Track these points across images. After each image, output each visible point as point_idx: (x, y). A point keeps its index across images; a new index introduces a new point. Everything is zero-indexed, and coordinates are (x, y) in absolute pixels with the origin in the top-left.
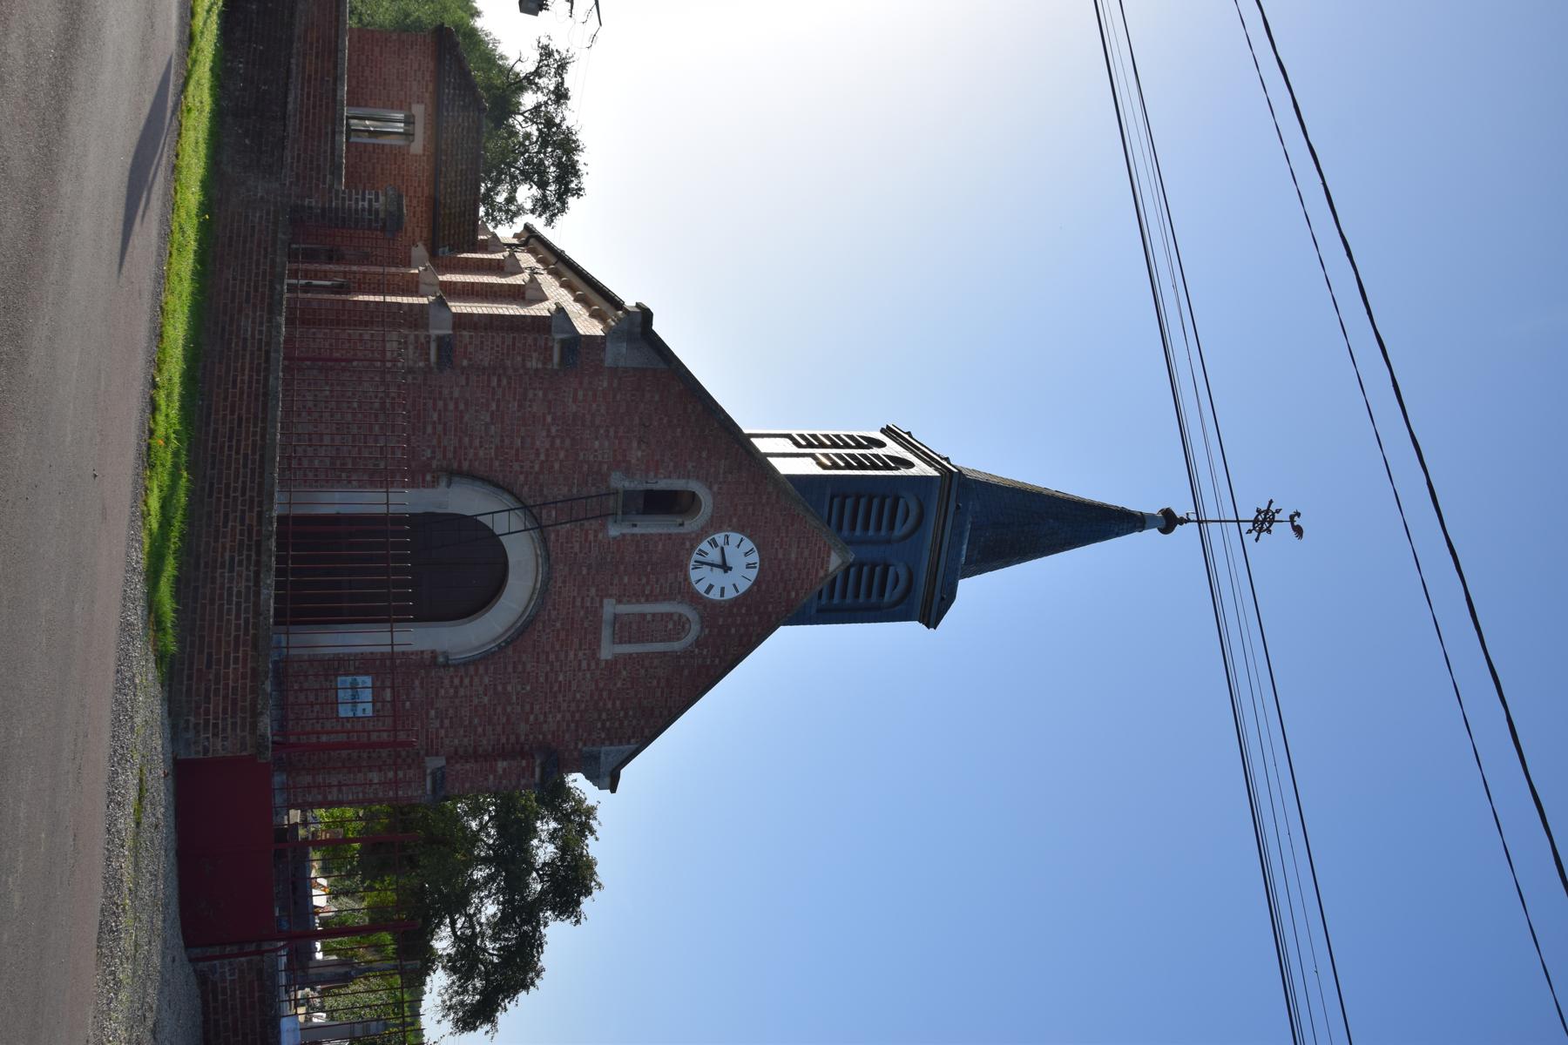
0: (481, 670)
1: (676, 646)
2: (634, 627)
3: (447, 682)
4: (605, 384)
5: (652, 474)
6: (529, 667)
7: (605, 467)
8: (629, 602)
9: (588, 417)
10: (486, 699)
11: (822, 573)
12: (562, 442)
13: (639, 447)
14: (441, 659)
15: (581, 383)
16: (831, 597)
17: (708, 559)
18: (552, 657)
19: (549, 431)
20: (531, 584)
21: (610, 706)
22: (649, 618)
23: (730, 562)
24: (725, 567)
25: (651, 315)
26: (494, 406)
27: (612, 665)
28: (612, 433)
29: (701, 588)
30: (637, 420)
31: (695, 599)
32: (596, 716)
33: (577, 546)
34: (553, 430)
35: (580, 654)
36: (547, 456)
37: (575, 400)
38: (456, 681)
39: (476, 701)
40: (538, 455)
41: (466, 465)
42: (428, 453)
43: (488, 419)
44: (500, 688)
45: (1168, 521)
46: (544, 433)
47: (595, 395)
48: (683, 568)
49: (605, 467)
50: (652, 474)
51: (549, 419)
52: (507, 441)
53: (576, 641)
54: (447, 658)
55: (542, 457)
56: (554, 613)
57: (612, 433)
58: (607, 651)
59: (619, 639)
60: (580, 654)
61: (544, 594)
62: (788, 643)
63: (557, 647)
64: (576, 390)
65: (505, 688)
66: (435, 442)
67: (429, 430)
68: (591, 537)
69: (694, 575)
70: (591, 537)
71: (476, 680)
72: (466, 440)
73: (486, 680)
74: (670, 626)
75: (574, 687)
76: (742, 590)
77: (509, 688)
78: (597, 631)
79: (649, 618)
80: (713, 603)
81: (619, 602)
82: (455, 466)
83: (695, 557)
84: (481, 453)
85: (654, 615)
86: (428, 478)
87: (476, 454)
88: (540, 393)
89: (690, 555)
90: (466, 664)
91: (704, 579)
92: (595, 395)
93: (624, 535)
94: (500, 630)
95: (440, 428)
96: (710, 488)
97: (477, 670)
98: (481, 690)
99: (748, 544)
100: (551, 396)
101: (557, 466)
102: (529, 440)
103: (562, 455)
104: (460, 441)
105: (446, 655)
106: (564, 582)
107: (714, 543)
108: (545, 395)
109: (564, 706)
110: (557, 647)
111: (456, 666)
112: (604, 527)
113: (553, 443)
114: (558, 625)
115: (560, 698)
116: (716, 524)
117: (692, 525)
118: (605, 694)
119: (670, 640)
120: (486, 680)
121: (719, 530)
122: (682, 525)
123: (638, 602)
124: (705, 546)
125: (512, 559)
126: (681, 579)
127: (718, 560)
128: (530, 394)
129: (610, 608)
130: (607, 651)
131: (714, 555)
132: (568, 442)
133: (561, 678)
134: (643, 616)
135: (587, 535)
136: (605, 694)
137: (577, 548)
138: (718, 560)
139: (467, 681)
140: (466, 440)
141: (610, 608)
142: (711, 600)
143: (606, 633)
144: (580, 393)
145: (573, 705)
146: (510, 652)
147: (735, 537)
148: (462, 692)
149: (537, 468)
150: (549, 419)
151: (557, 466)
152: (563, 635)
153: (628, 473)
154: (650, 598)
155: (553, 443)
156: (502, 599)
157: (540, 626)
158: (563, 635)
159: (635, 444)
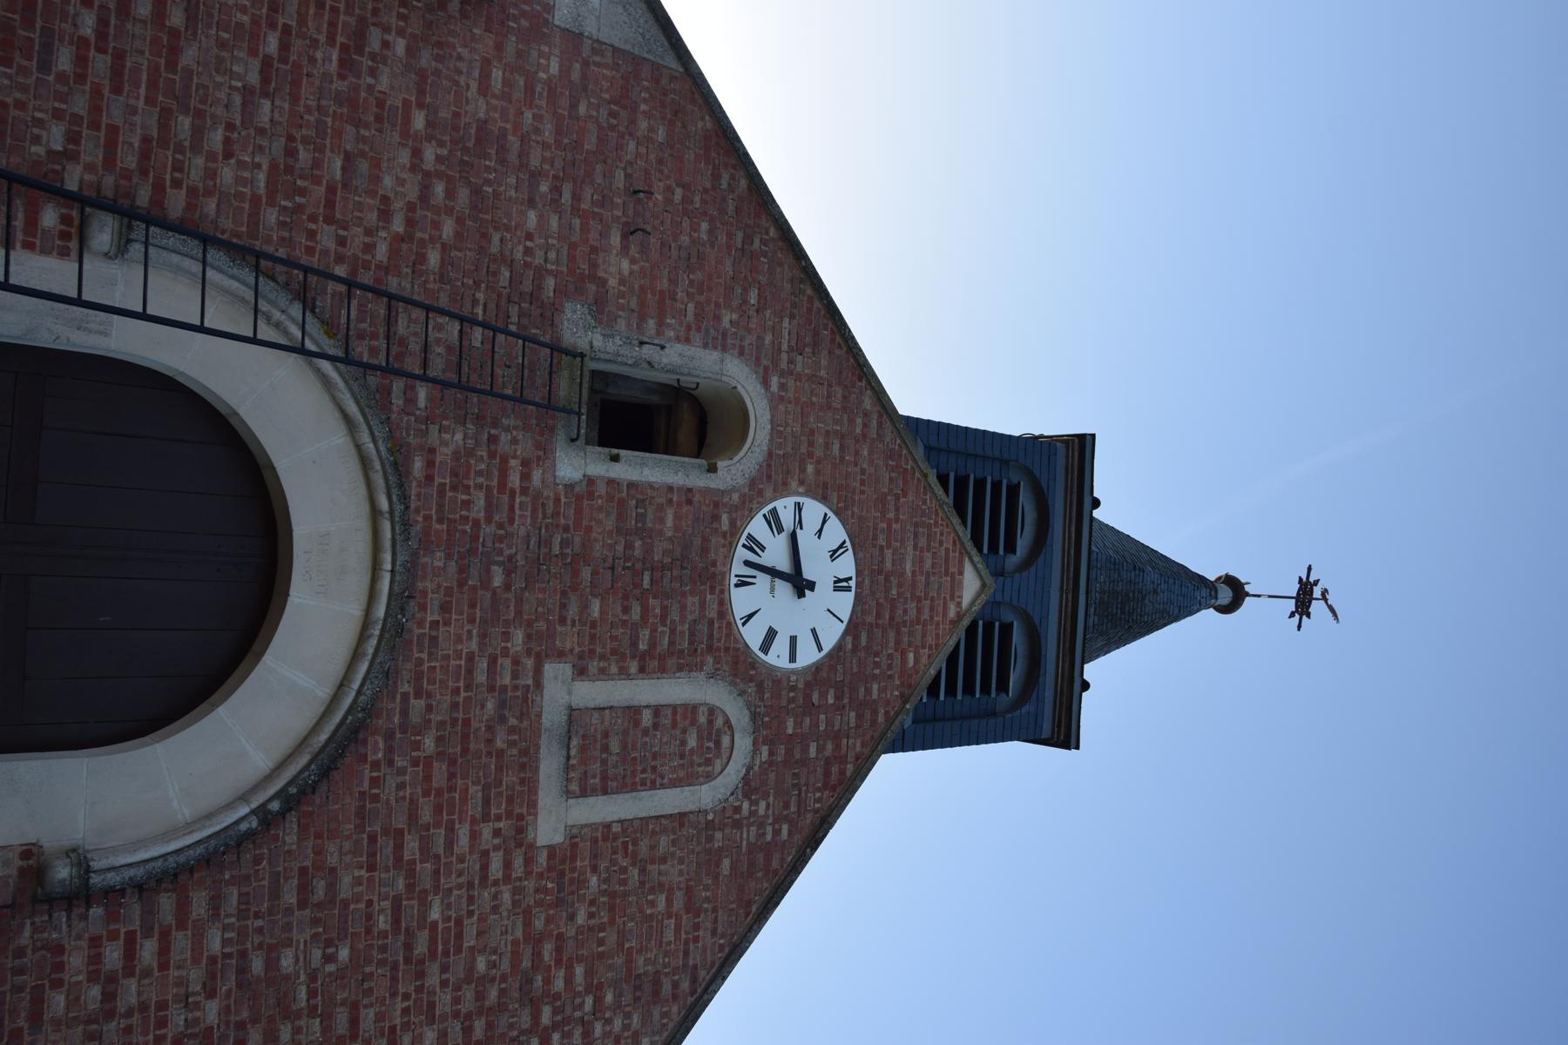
0: (199, 904)
1: (705, 796)
2: (615, 747)
3: (76, 961)
4: (554, 68)
5: (651, 324)
6: (345, 888)
7: (550, 283)
8: (603, 674)
9: (514, 142)
10: (211, 1011)
11: (952, 614)
12: (450, 194)
13: (625, 249)
14: (62, 872)
15: (499, 47)
16: (951, 691)
17: (766, 559)
18: (411, 846)
19: (417, 153)
20: (356, 610)
21: (559, 984)
22: (647, 718)
23: (808, 574)
24: (801, 586)
25: (1227, 576)
26: (272, 44)
27: (563, 856)
28: (566, 197)
29: (752, 636)
30: (619, 180)
31: (740, 666)
32: (525, 1020)
33: (480, 501)
34: (429, 154)
35: (486, 831)
36: (410, 223)
37: (484, 90)
38: (113, 955)
39: (178, 1019)
40: (385, 215)
41: (176, 204)
42: (56, 137)
43: (254, 78)
44: (257, 965)
46: (404, 157)
47: (530, 90)
48: (713, 581)
49: (550, 283)
50: (651, 324)
51: (419, 121)
52: (304, 156)
53: (475, 791)
54: (83, 865)
55: (398, 226)
56: (418, 705)
57: (566, 197)
59: (581, 786)
60: (486, 831)
61: (391, 637)
62: (901, 784)
63: (426, 815)
64: (486, 64)
65: (272, 964)
66: (80, 105)
67: (64, 60)
68: (515, 480)
69: (741, 602)
70: (515, 480)
71: (181, 942)
72: (184, 123)
73: (215, 943)
74: (692, 742)
75: (469, 941)
76: (829, 643)
77: (287, 962)
78: (528, 763)
79: (647, 718)
81: (581, 672)
82: (143, 197)
83: (741, 553)
84: (227, 174)
85: (657, 710)
86: (49, 217)
87: (211, 174)
88: (400, 46)
89: (731, 548)
90: (150, 884)
92: (530, 90)
93: (591, 481)
94: (261, 762)
95: (100, 64)
96: (765, 383)
97: (183, 907)
98: (196, 976)
100: (425, 59)
101: (434, 258)
102: (363, 166)
103: (448, 229)
104: (164, 125)
105: (79, 858)
106: (445, 608)
107: (774, 521)
108: (411, 51)
109: (444, 1000)
110: (426, 815)
111: (112, 895)
112: (544, 452)
113: (426, 190)
114: (429, 743)
115: (433, 980)
116: (775, 477)
117: (734, 471)
118: (548, 949)
119: (690, 779)
120: (215, 943)
121: (782, 490)
122: (615, 459)
123: (624, 673)
124: (757, 527)
126: (712, 613)
127: (784, 565)
128: (374, 40)
129: (562, 691)
131: (776, 553)
132: (463, 195)
133: (435, 914)
134: (633, 711)
135: (504, 473)
136: (548, 949)
137: (478, 509)
138: (784, 565)
139: (148, 951)
140: (184, 123)
141: (562, 691)
142: (772, 669)
143: (549, 766)
144: (497, 74)
145: (469, 994)
146: (289, 835)
147: (814, 510)
148: (130, 991)
149: (382, 253)
150: (419, 121)
151: (434, 258)
152: (440, 771)
153: (600, 310)
154: (652, 663)
155: (426, 190)
156: (268, 659)
157: (377, 747)
158: (440, 771)
159: (616, 239)
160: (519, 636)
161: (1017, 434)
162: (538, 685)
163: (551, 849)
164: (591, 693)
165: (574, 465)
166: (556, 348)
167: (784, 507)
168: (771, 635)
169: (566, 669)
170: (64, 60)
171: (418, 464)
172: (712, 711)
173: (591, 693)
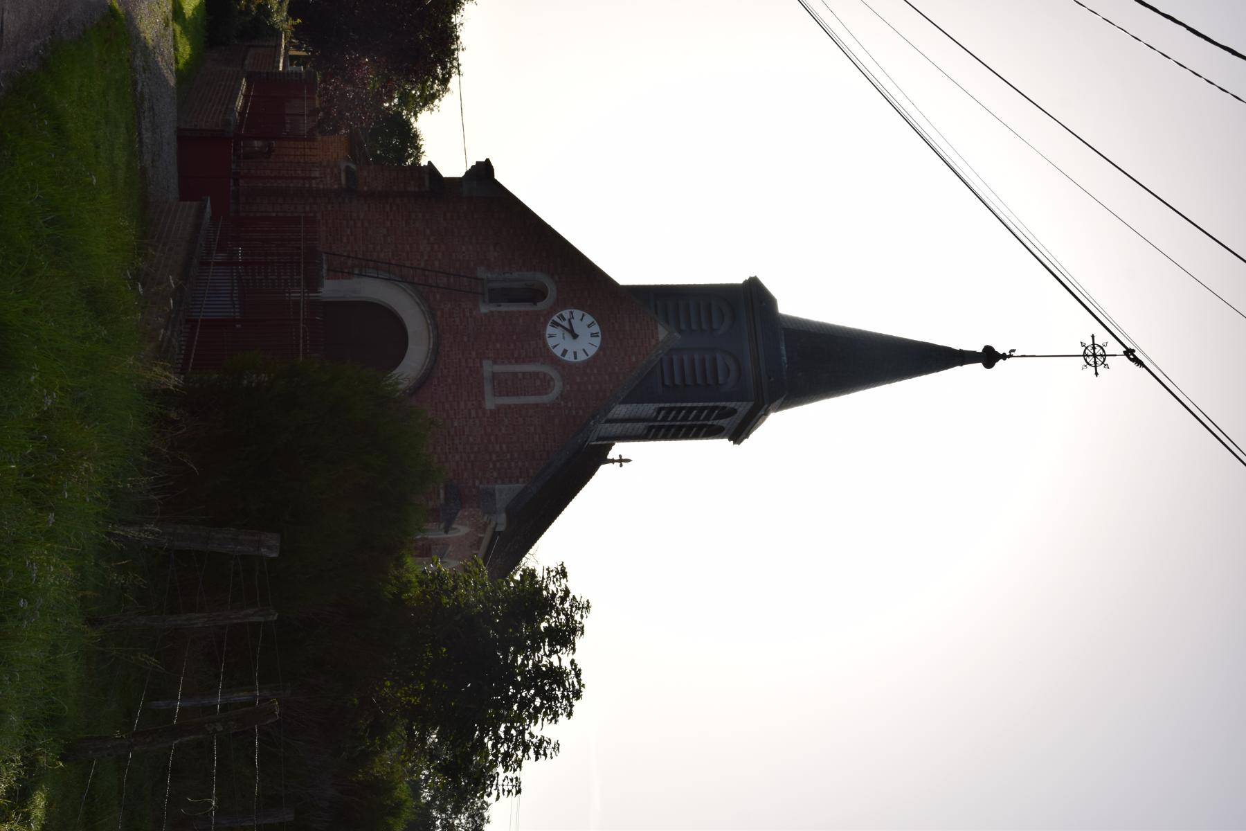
22: (520, 376)
23: (576, 331)
26: (388, 223)
29: (558, 352)
34: (432, 239)
45: (989, 357)
51: (428, 232)
58: (491, 403)
61: (436, 352)
67: (345, 240)
79: (520, 376)
80: (569, 364)
81: (495, 363)
85: (524, 374)
91: (557, 341)
99: (589, 319)
103: (440, 256)
114: (450, 380)
117: (542, 306)
118: (493, 438)
121: (565, 308)
125: (410, 330)
129: (488, 368)
130: (491, 403)
134: (515, 374)
141: (488, 368)
143: (488, 388)
147: (578, 313)
150: (428, 232)
154: (519, 360)
160: (474, 354)
161: (740, 281)
162: (482, 366)
163: (491, 411)
164: (499, 368)
165: (484, 309)
166: (477, 279)
167: (566, 313)
168: (575, 353)
169: (490, 362)
170: (345, 240)
171: (439, 313)
172: (545, 374)
173: (499, 368)
